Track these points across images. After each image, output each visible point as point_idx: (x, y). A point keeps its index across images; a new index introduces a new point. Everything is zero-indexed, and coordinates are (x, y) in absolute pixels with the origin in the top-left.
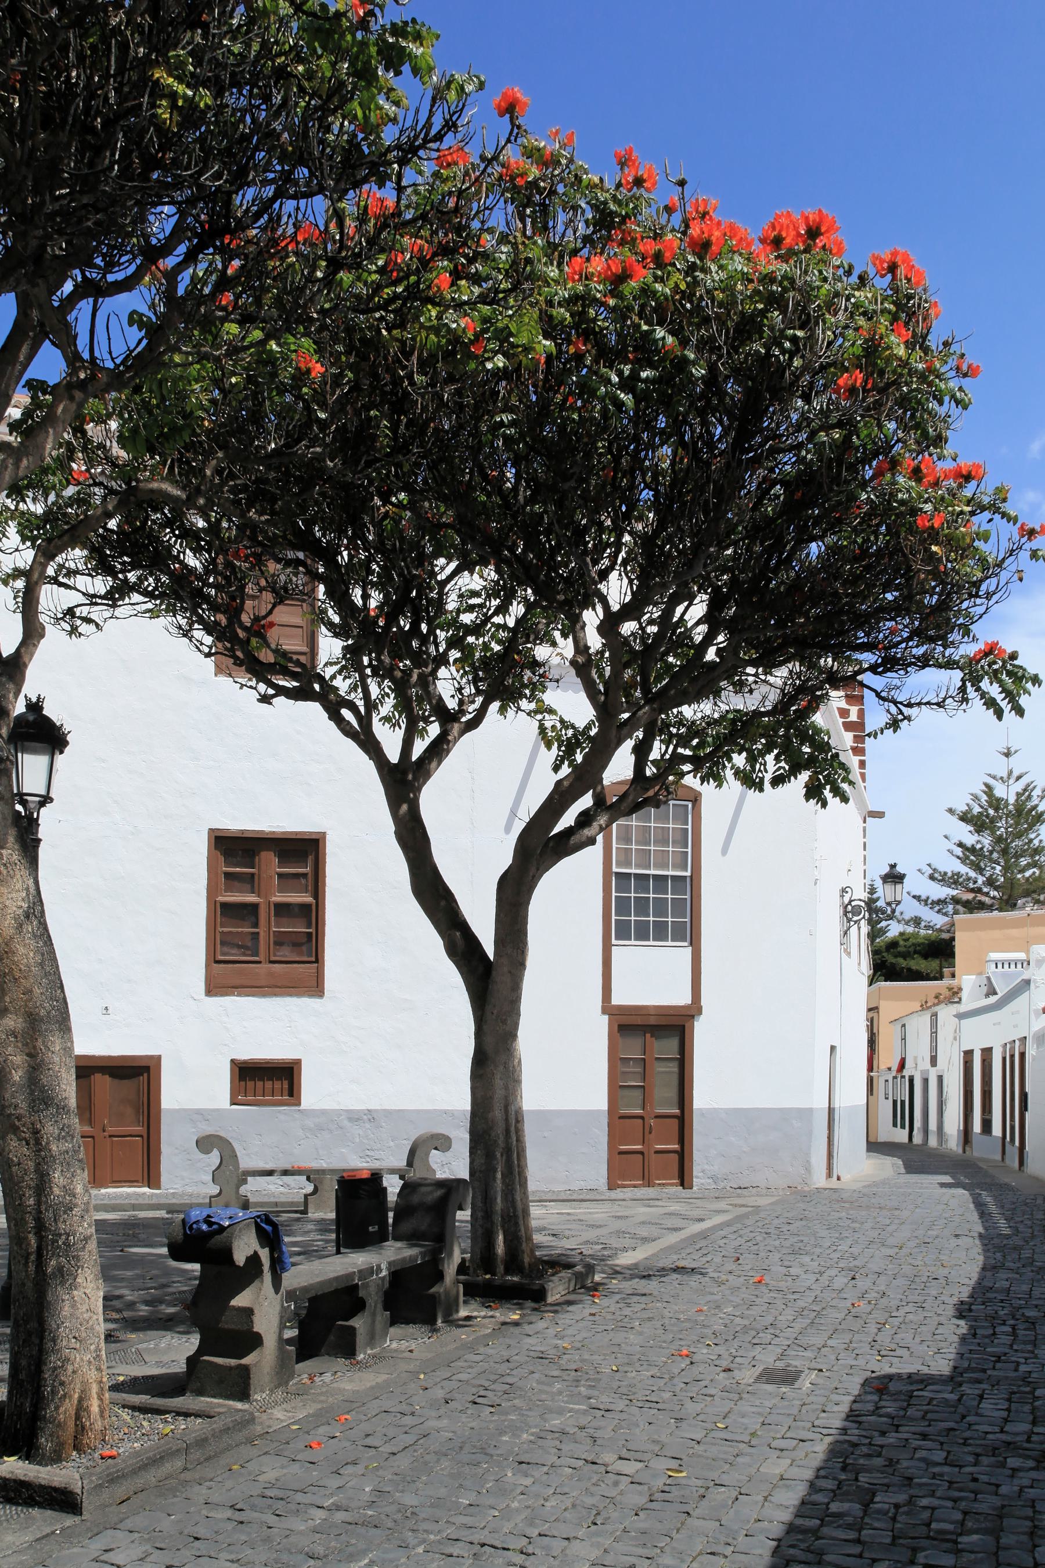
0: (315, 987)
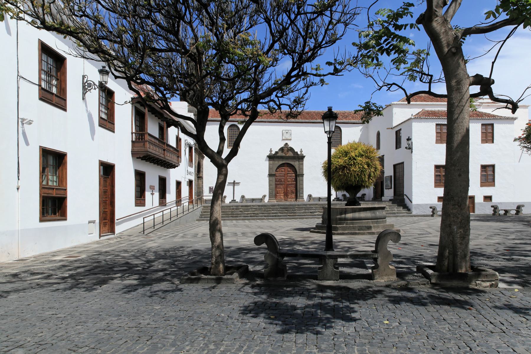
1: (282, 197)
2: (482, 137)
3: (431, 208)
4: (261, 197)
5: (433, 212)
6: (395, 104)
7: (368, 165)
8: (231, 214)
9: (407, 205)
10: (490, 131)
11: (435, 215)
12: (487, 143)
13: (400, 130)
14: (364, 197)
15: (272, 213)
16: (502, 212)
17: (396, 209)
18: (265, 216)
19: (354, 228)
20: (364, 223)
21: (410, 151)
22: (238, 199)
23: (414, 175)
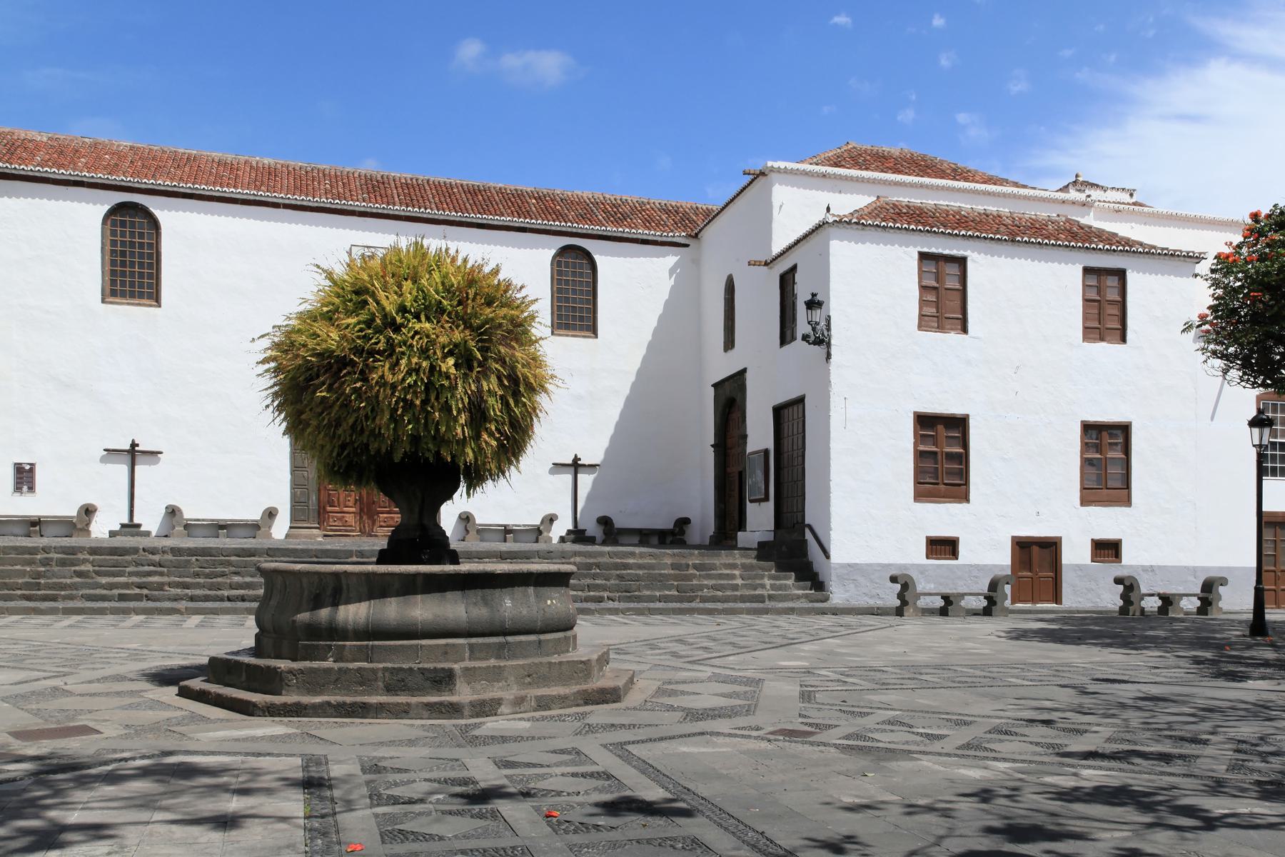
0: (965, 498)
1: (350, 519)
2: (1086, 318)
3: (894, 579)
4: (255, 515)
6: (779, 170)
7: (465, 361)
8: (27, 586)
9: (816, 567)
10: (1113, 295)
11: (909, 611)
12: (1102, 339)
13: (794, 268)
14: (683, 532)
15: (231, 587)
16: (1152, 604)
17: (767, 582)
18: (192, 599)
19: (365, 680)
20: (427, 655)
21: (819, 350)
22: (150, 520)
23: (835, 446)
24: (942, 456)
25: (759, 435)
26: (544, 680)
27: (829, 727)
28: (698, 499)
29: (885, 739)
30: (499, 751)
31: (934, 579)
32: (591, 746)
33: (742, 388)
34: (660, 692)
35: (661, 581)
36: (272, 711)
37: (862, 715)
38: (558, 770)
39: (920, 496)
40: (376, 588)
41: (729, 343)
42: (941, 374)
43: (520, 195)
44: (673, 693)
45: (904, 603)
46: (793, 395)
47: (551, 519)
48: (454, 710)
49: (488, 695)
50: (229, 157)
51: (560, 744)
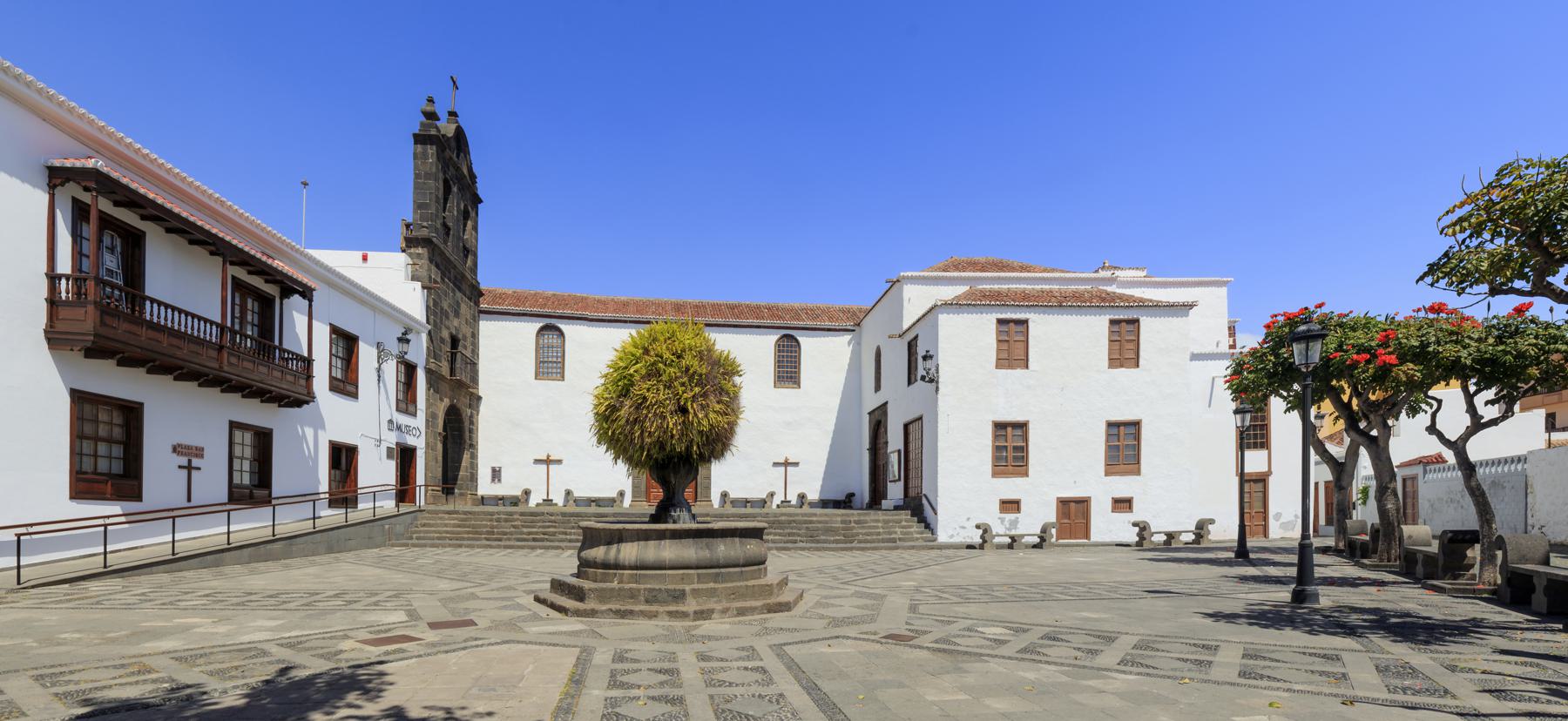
0: (1026, 475)
3: (978, 527)
5: (982, 537)
19: (633, 595)
22: (559, 500)
24: (1011, 446)
25: (895, 440)
26: (743, 597)
27: (925, 633)
28: (861, 484)
29: (965, 643)
30: (699, 647)
31: (1000, 527)
32: (761, 645)
33: (885, 414)
34: (818, 604)
35: (834, 531)
36: (578, 613)
37: (949, 623)
38: (736, 664)
39: (995, 474)
40: (644, 536)
41: (878, 388)
42: (1011, 396)
43: (758, 307)
44: (828, 605)
45: (985, 541)
46: (916, 415)
47: (772, 495)
48: (684, 615)
49: (705, 607)
50: (603, 298)
51: (742, 643)
